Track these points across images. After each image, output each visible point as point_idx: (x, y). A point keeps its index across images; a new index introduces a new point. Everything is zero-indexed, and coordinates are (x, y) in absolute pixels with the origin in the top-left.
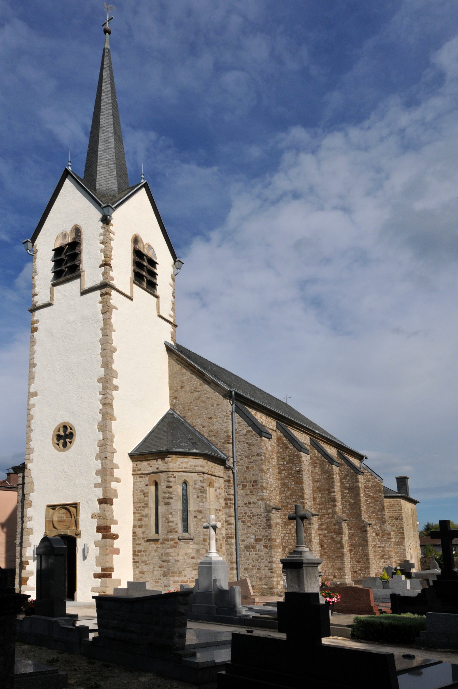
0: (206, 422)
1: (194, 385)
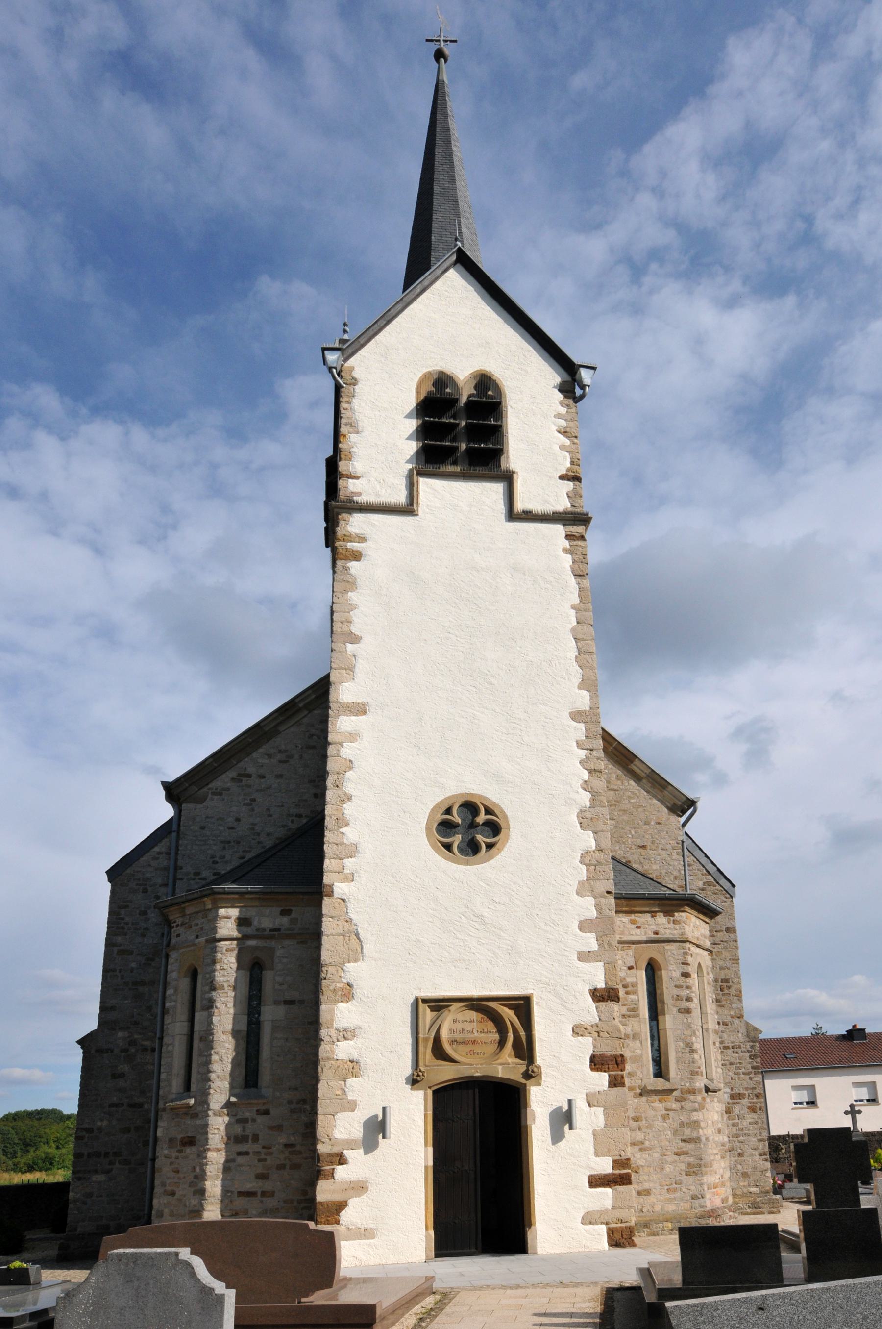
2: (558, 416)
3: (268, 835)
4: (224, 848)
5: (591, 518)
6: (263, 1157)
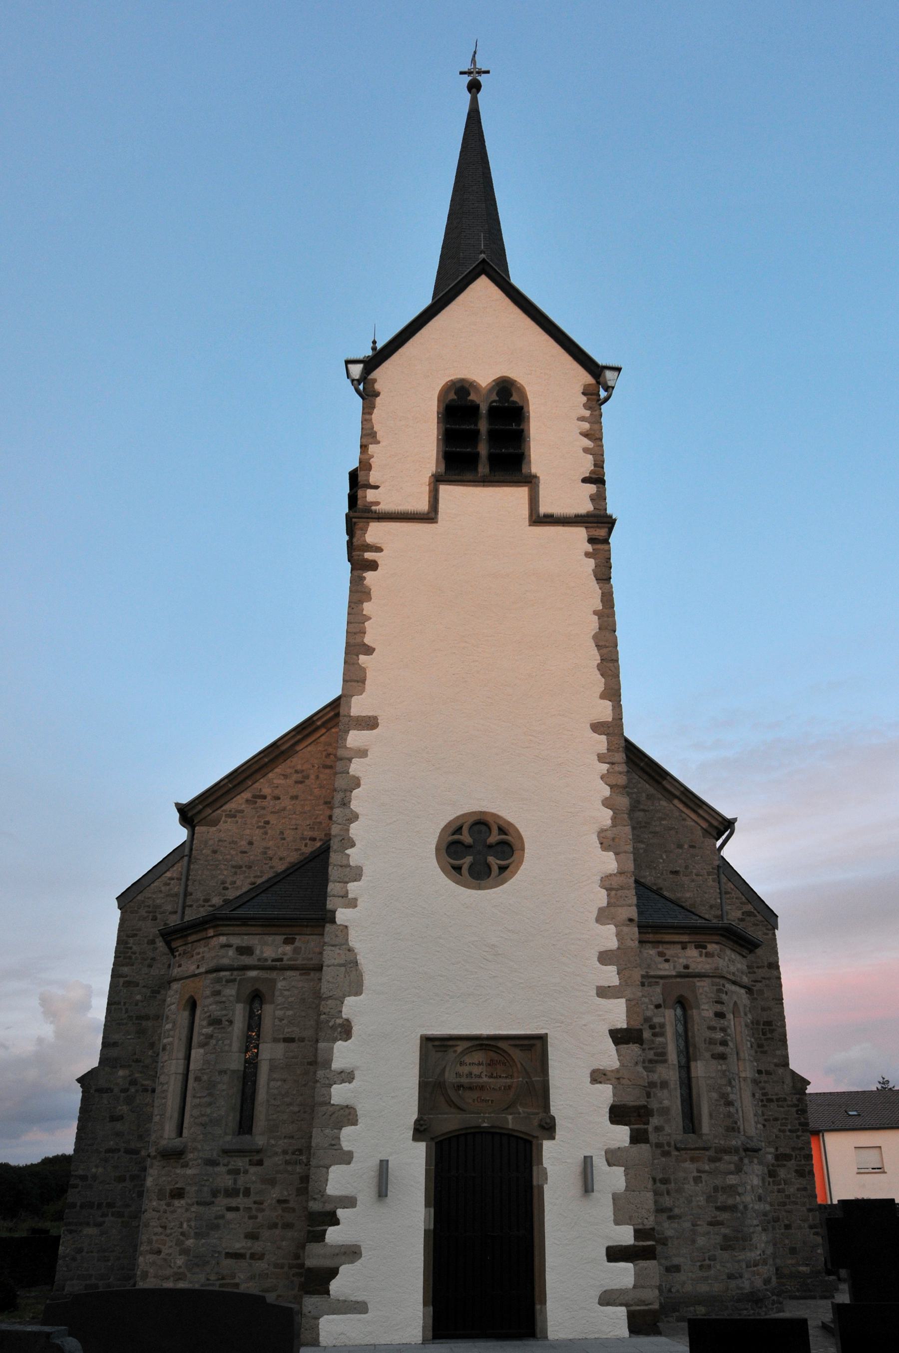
0: (665, 880)
1: (634, 796)
2: (582, 419)
3: (281, 859)
4: (235, 873)
5: (615, 520)
6: (254, 1213)
